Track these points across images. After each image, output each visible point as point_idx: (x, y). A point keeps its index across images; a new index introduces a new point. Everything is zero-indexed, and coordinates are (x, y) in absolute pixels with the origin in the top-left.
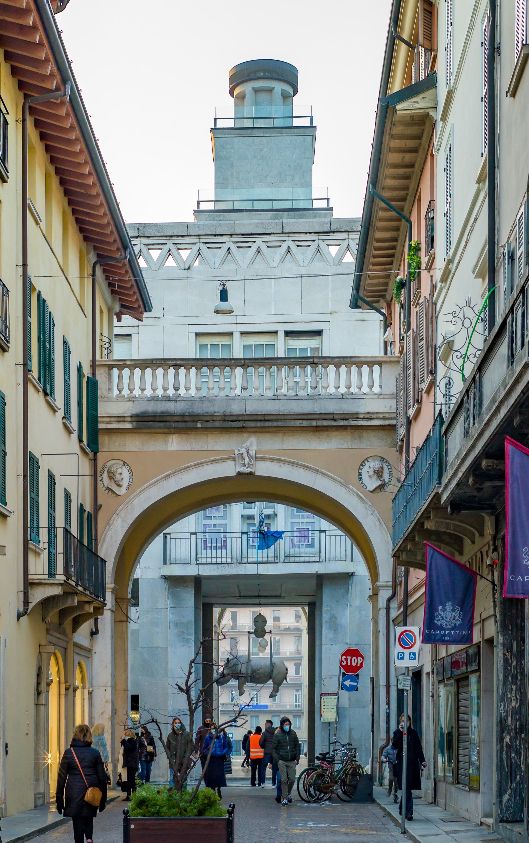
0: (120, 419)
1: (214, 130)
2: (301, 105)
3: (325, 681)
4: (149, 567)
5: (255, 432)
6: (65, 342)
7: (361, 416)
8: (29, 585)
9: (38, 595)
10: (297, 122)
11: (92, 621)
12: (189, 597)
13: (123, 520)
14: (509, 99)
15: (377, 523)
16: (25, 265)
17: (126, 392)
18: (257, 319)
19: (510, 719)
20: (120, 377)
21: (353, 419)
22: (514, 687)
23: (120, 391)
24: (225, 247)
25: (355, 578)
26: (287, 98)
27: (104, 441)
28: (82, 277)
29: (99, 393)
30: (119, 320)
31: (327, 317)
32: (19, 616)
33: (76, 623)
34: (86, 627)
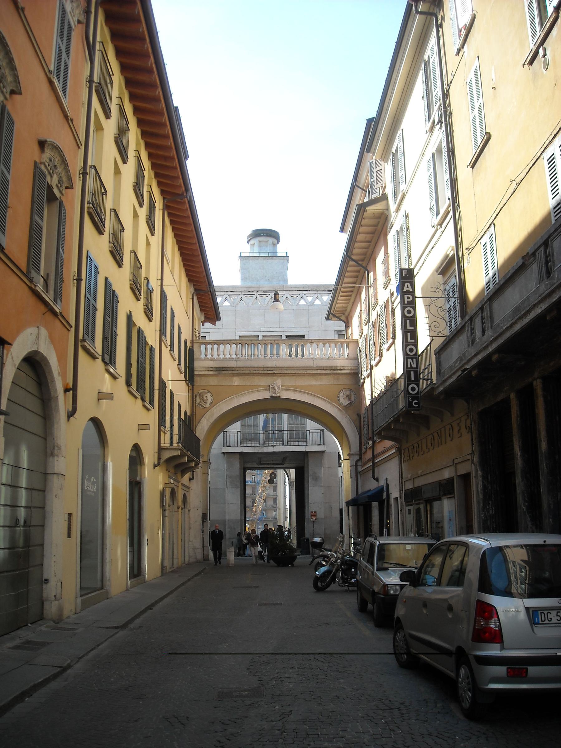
0: (208, 369)
1: (241, 257)
2: (281, 248)
3: (311, 505)
4: (217, 447)
5: (281, 376)
6: (179, 327)
7: (339, 368)
8: (160, 449)
9: (166, 455)
10: (279, 254)
11: (191, 473)
12: (237, 464)
13: (208, 420)
14: (73, 512)
15: (349, 422)
16: (162, 279)
17: (209, 356)
18: (271, 330)
19: (489, 521)
20: (206, 349)
21: (334, 370)
22: (490, 502)
23: (206, 356)
24: (255, 296)
25: (325, 453)
26: (274, 245)
27: (197, 379)
28: (187, 298)
29: (195, 357)
30: (203, 325)
31: (307, 329)
32: (155, 466)
33: (183, 473)
34: (187, 476)
